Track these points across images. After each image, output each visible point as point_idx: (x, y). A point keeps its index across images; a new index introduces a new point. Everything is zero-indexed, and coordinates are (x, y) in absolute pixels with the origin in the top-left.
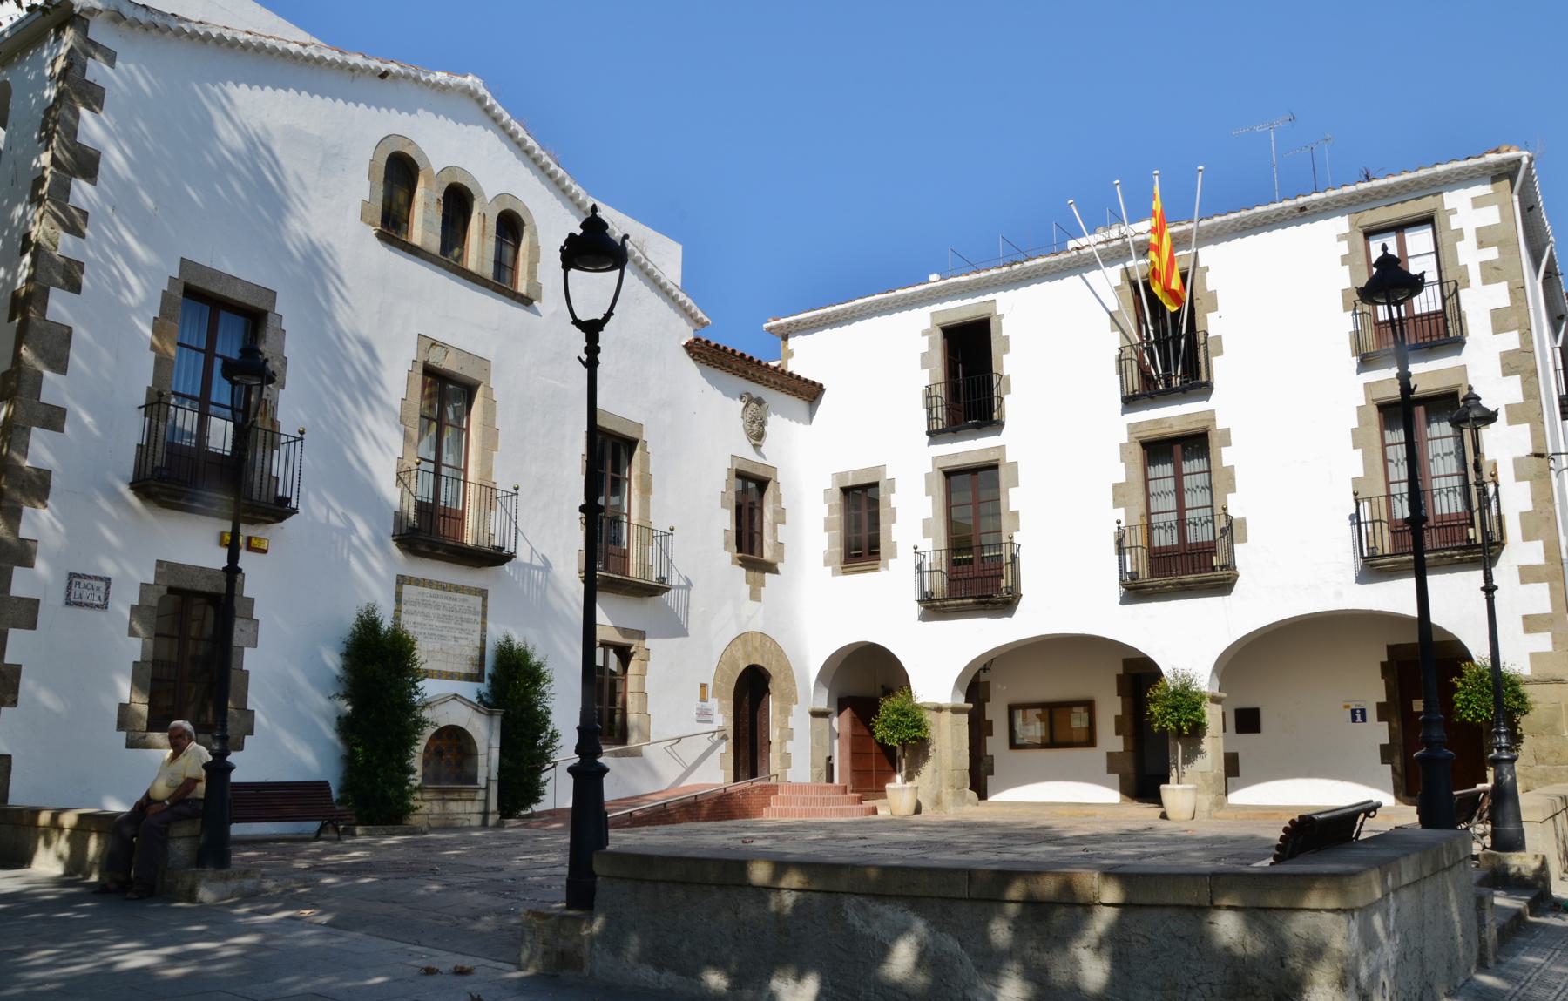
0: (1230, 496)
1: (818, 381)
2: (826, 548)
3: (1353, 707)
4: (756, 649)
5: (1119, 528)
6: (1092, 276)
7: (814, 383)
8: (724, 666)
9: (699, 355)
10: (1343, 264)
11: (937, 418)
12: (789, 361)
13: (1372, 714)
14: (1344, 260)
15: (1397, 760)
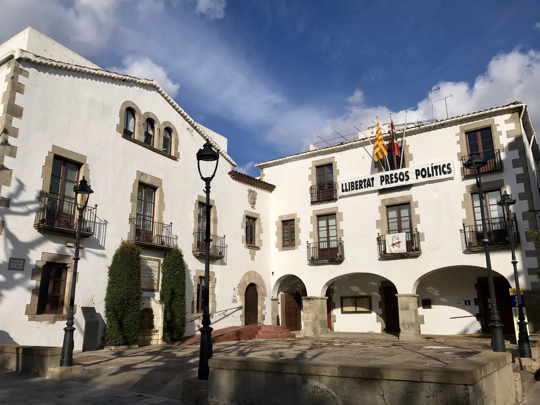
0: (418, 225)
1: (273, 184)
2: (277, 242)
4: (253, 277)
5: (379, 236)
6: (366, 147)
11: (314, 196)
13: (472, 302)
14: (458, 143)
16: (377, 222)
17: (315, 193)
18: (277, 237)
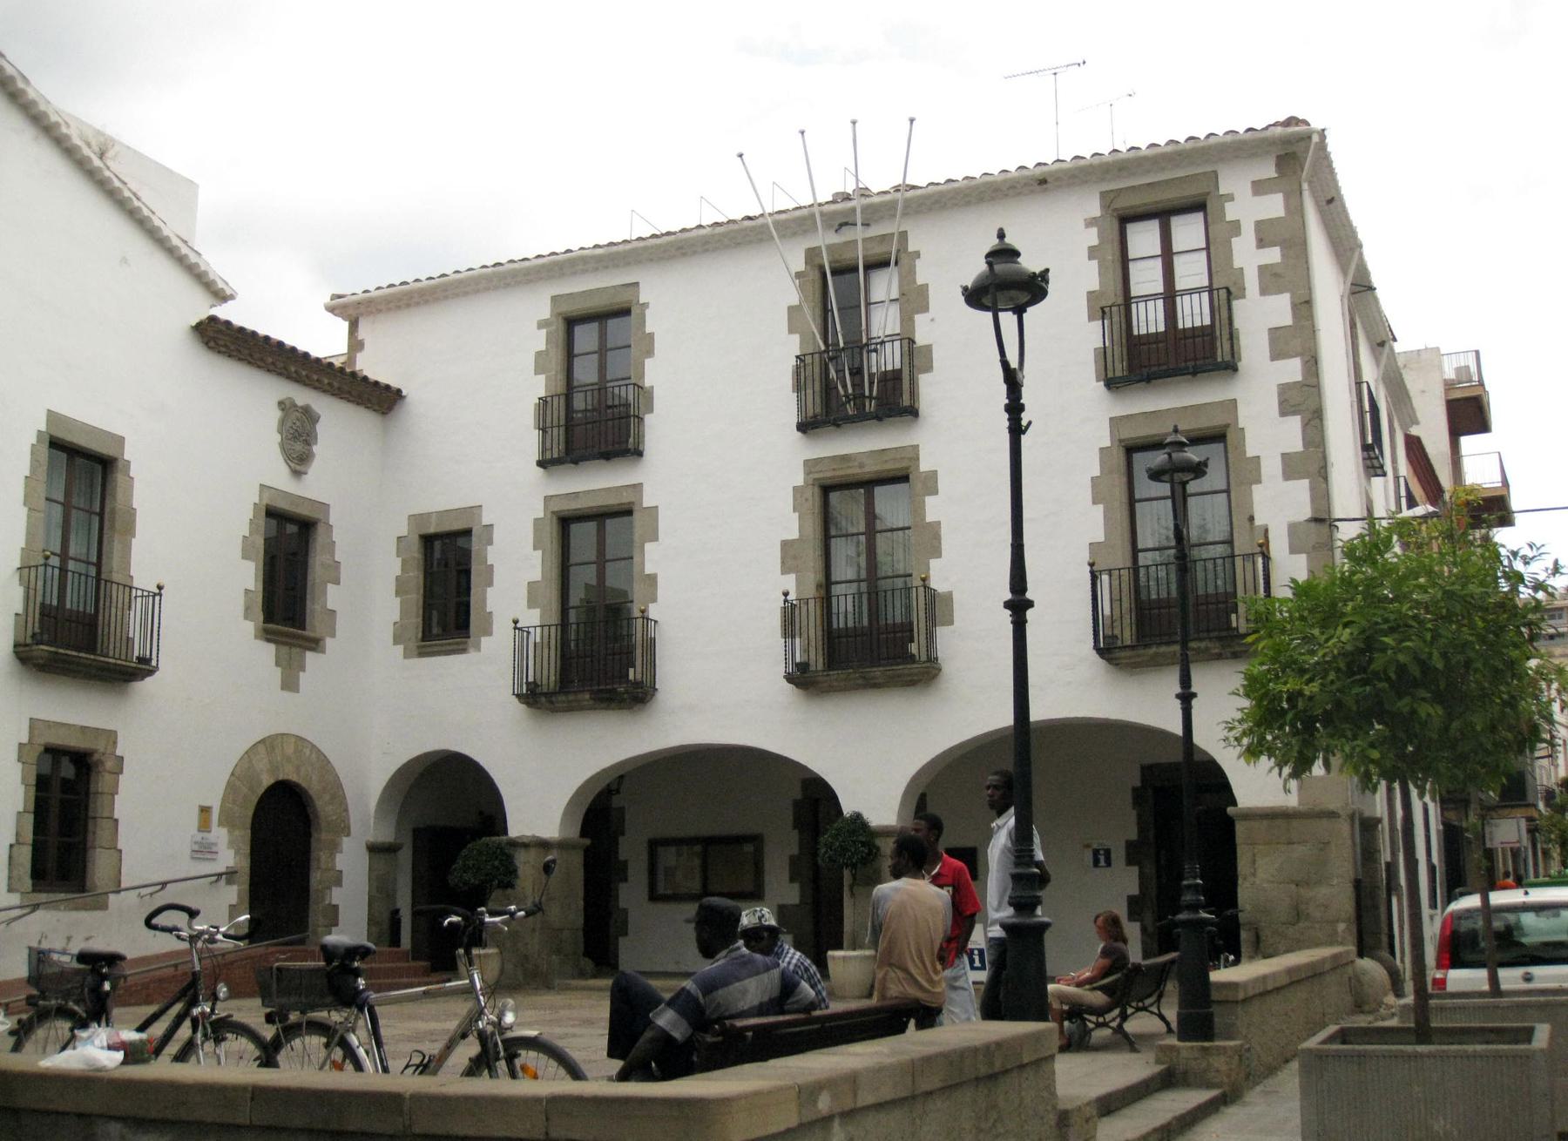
0: (934, 563)
1: (394, 384)
3: (1095, 846)
5: (786, 601)
7: (388, 387)
8: (238, 783)
9: (214, 339)
10: (1090, 258)
12: (359, 355)
13: (1119, 855)
14: (1093, 252)
15: (1149, 917)
16: (786, 545)
17: (548, 424)
18: (399, 599)
